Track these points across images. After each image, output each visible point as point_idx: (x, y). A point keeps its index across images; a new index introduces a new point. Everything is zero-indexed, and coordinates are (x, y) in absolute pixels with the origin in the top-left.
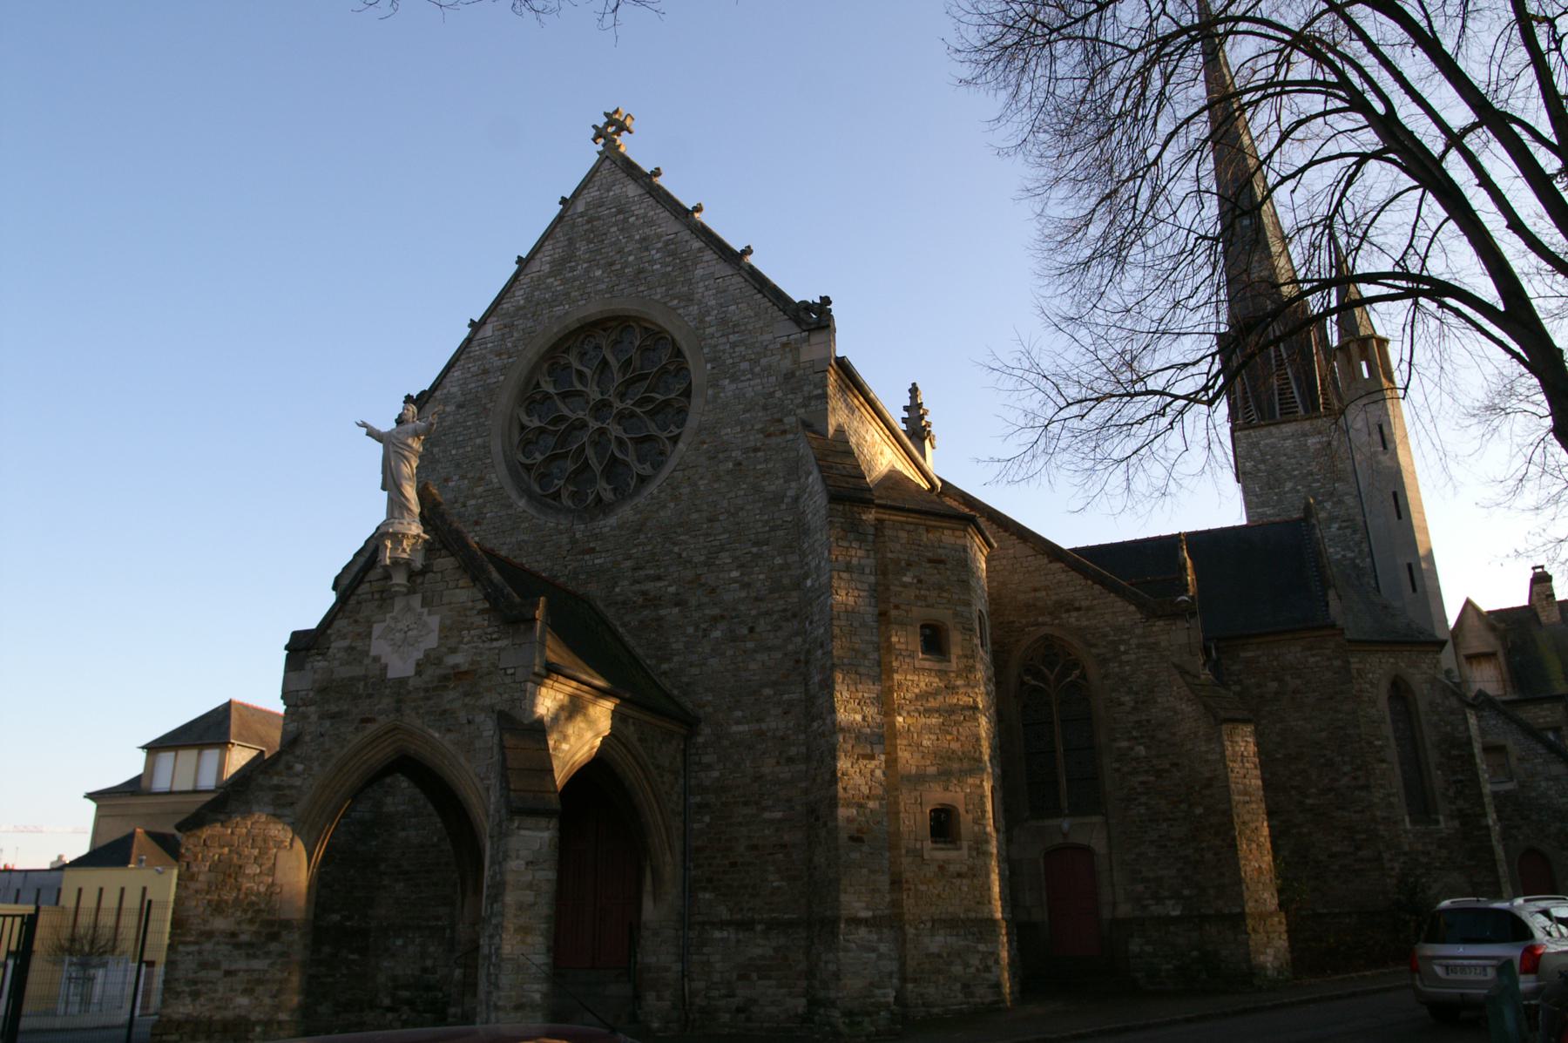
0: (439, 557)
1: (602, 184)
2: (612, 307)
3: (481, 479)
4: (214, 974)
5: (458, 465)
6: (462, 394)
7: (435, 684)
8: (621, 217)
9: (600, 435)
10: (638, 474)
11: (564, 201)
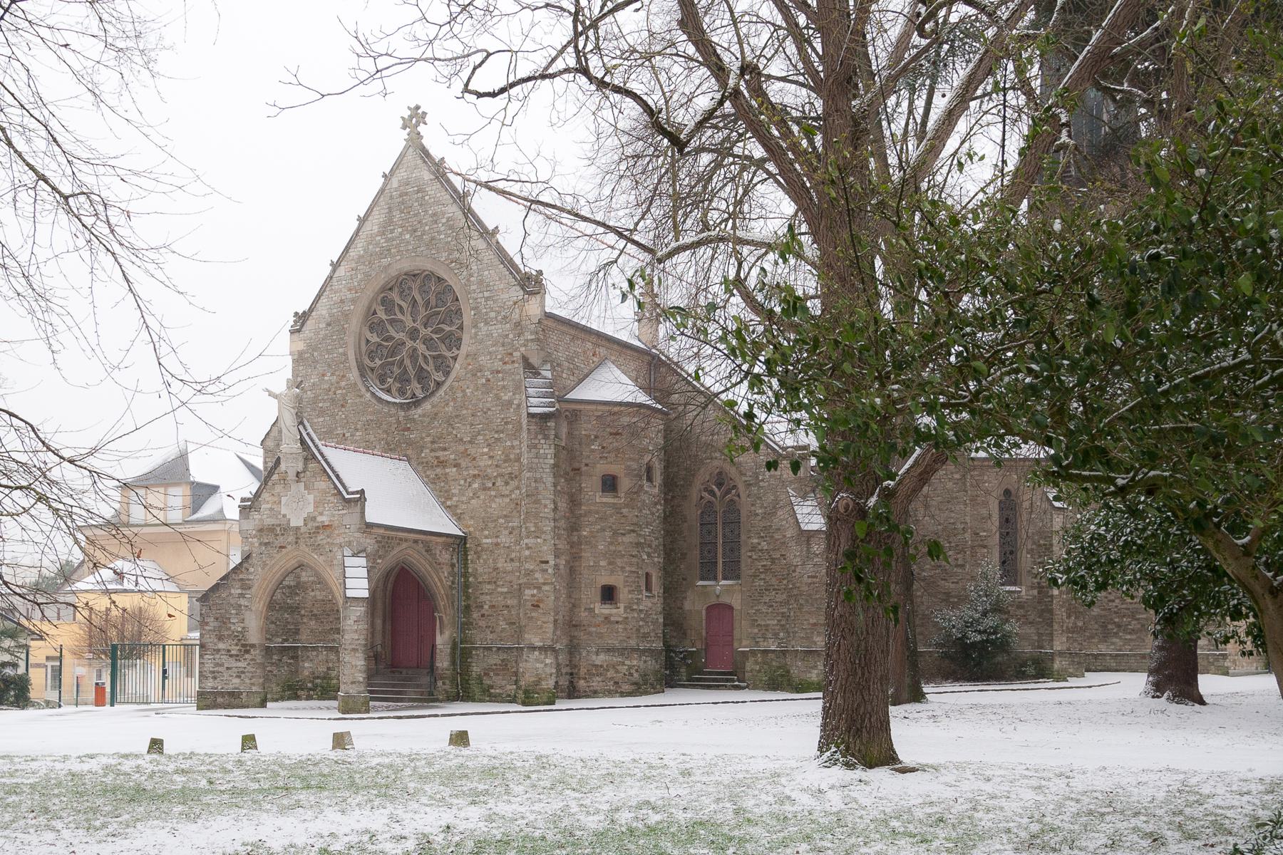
3: (343, 376)
4: (220, 669)
5: (329, 366)
8: (420, 195)
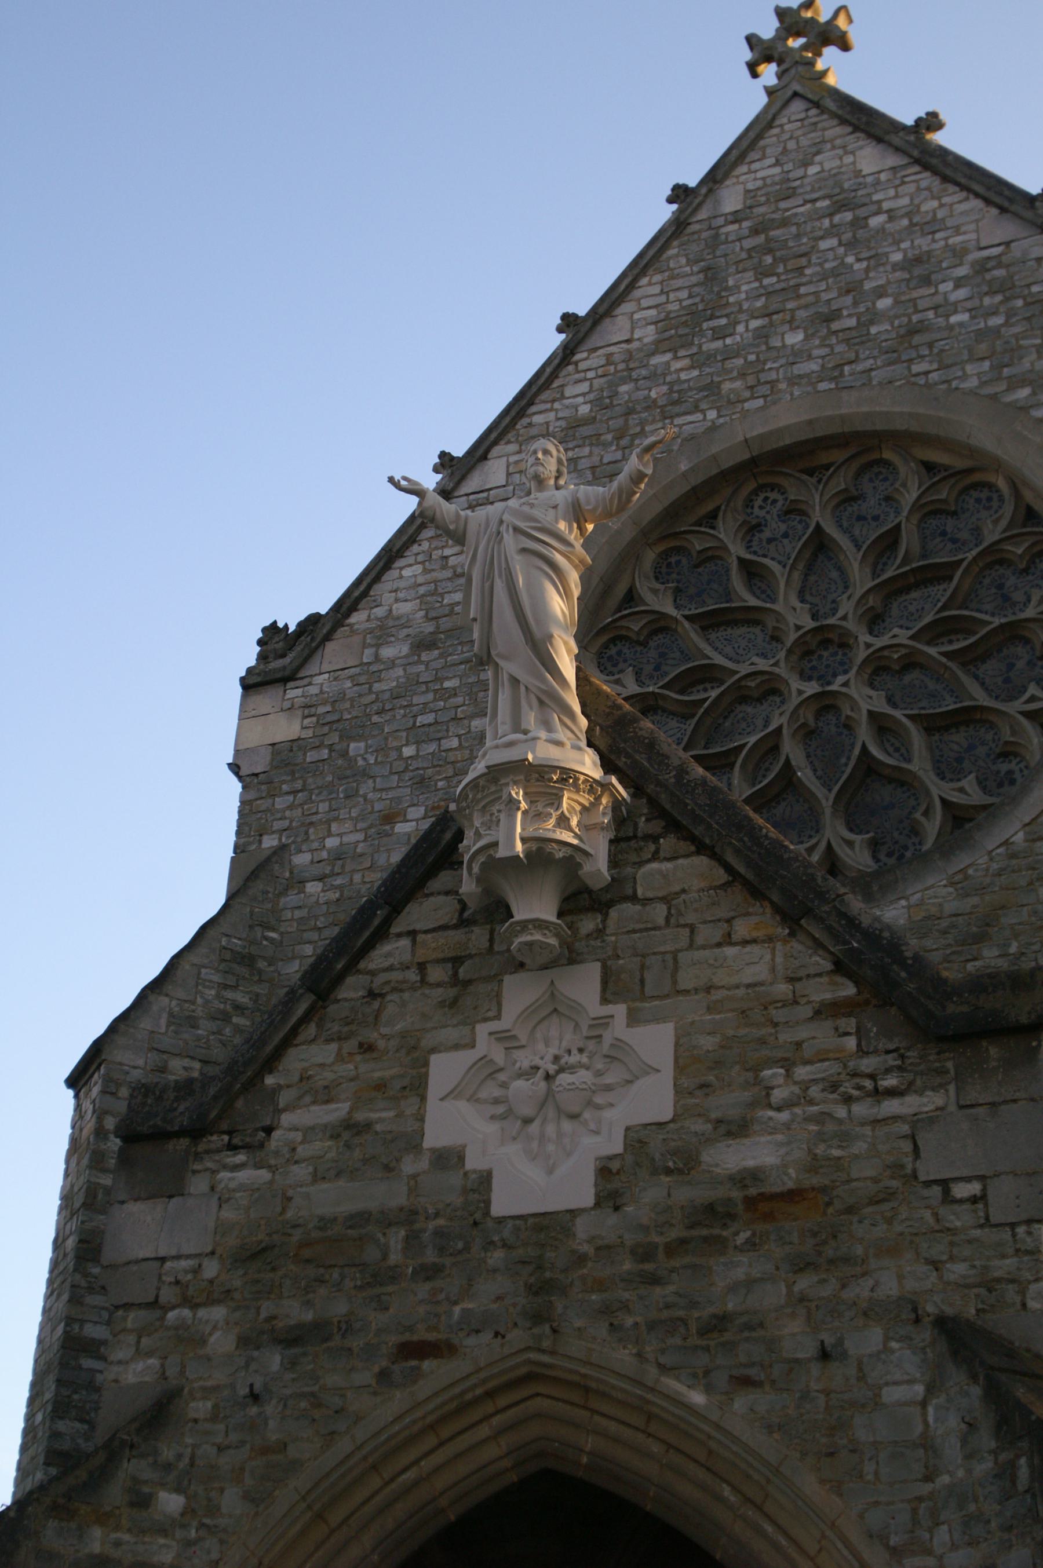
0: (655, 857)
1: (785, 151)
2: (843, 411)
6: (428, 618)
7: (674, 1234)
9: (819, 714)
10: (943, 800)
11: (679, 194)
